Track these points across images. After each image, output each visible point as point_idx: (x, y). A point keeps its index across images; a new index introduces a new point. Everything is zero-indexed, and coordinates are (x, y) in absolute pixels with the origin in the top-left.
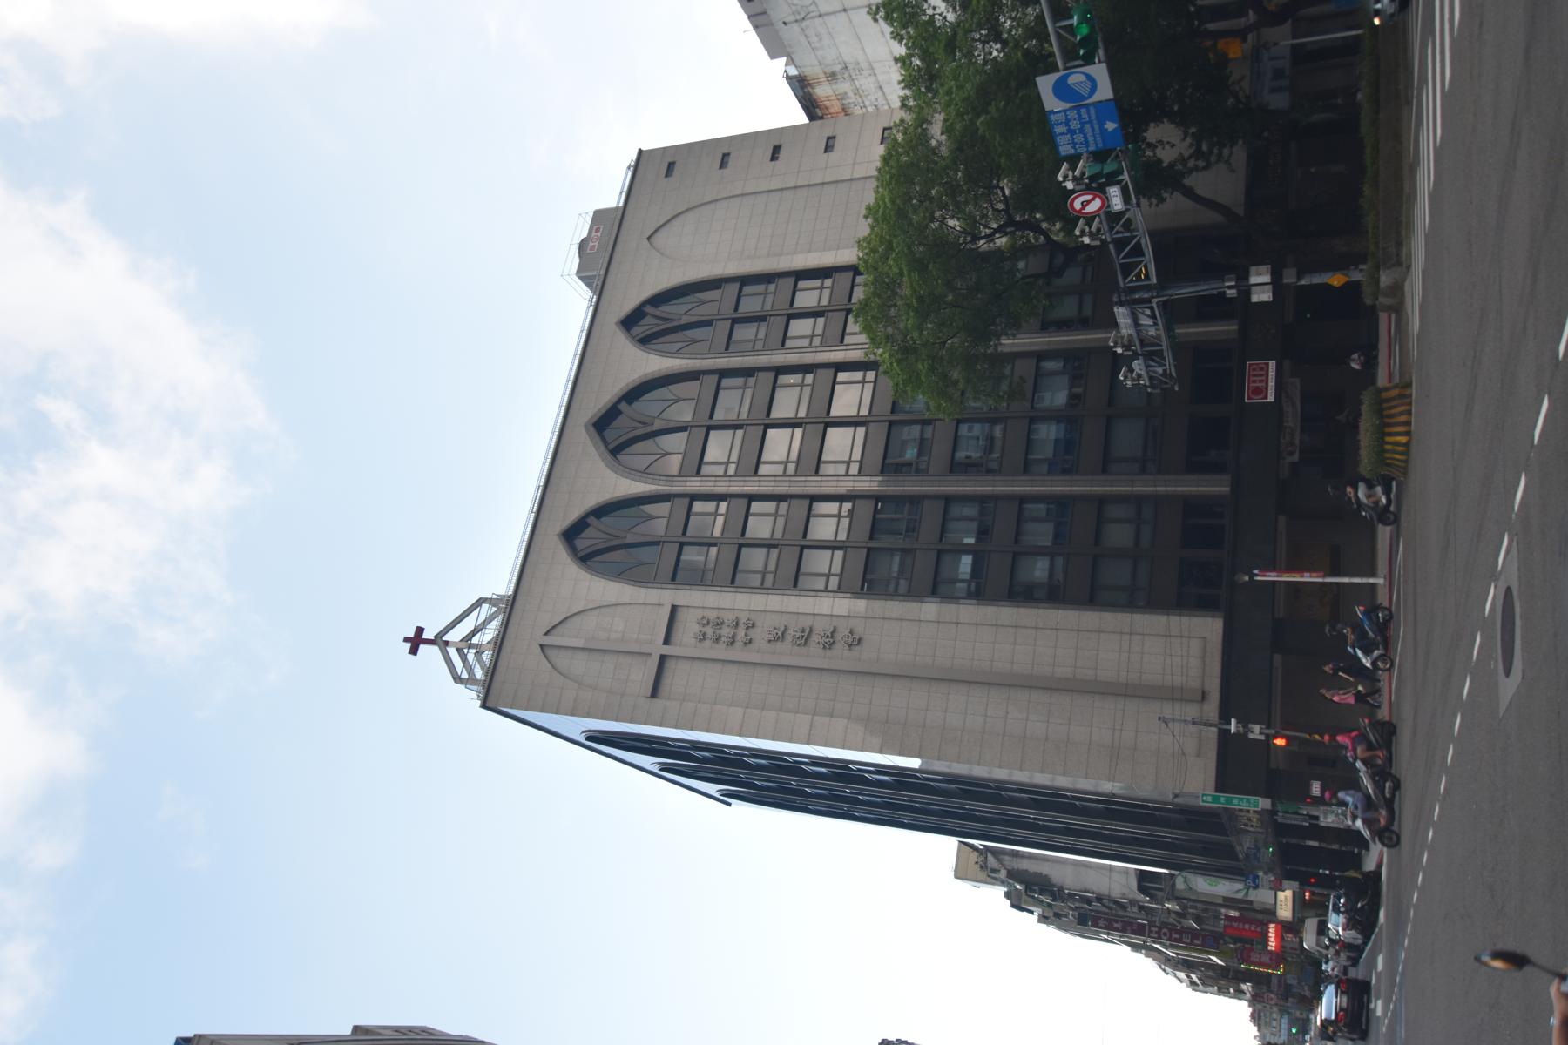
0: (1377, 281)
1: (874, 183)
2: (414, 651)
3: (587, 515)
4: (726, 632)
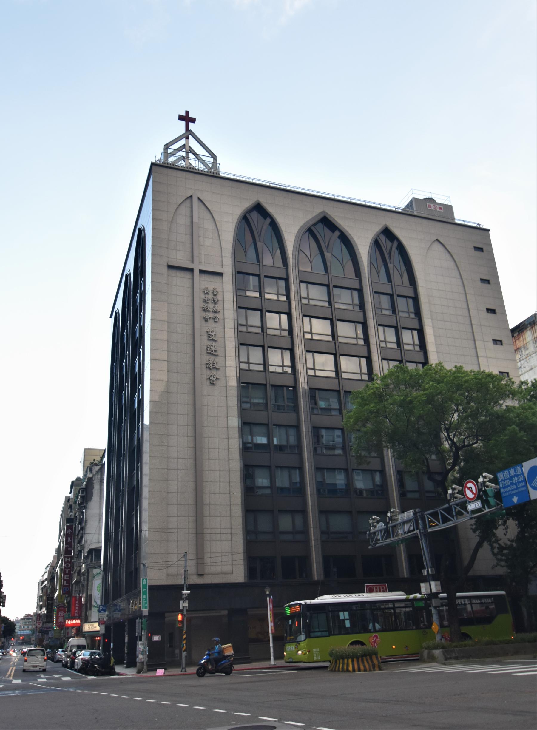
1: (476, 369)
2: (181, 118)
4: (211, 306)
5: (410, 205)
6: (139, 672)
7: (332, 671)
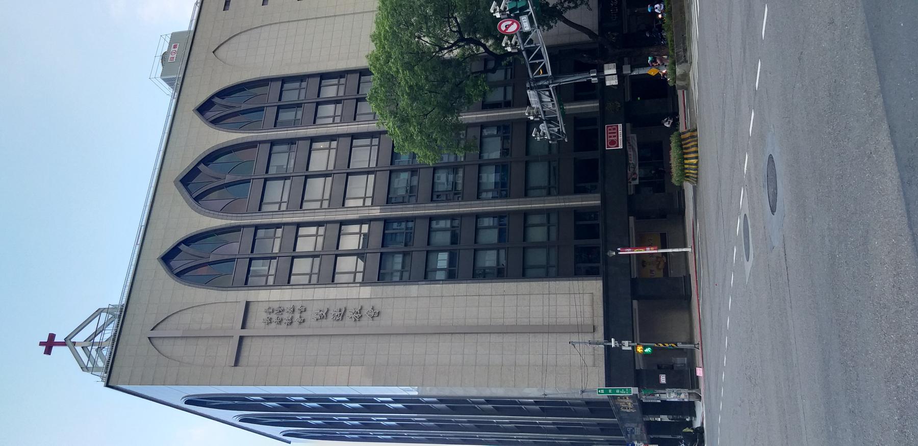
0: (675, 73)
1: (373, 17)
2: (48, 352)
3: (179, 244)
4: (286, 316)
5: (170, 82)
6: (699, 398)
7: (697, 181)
